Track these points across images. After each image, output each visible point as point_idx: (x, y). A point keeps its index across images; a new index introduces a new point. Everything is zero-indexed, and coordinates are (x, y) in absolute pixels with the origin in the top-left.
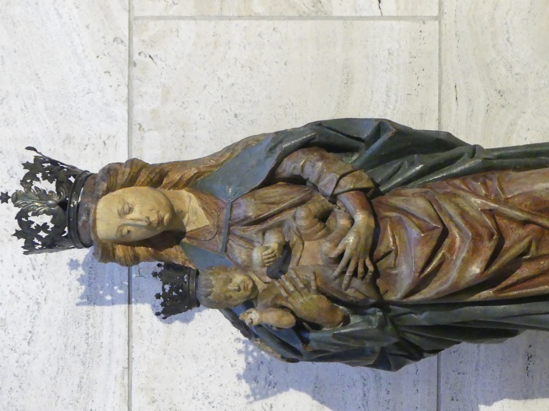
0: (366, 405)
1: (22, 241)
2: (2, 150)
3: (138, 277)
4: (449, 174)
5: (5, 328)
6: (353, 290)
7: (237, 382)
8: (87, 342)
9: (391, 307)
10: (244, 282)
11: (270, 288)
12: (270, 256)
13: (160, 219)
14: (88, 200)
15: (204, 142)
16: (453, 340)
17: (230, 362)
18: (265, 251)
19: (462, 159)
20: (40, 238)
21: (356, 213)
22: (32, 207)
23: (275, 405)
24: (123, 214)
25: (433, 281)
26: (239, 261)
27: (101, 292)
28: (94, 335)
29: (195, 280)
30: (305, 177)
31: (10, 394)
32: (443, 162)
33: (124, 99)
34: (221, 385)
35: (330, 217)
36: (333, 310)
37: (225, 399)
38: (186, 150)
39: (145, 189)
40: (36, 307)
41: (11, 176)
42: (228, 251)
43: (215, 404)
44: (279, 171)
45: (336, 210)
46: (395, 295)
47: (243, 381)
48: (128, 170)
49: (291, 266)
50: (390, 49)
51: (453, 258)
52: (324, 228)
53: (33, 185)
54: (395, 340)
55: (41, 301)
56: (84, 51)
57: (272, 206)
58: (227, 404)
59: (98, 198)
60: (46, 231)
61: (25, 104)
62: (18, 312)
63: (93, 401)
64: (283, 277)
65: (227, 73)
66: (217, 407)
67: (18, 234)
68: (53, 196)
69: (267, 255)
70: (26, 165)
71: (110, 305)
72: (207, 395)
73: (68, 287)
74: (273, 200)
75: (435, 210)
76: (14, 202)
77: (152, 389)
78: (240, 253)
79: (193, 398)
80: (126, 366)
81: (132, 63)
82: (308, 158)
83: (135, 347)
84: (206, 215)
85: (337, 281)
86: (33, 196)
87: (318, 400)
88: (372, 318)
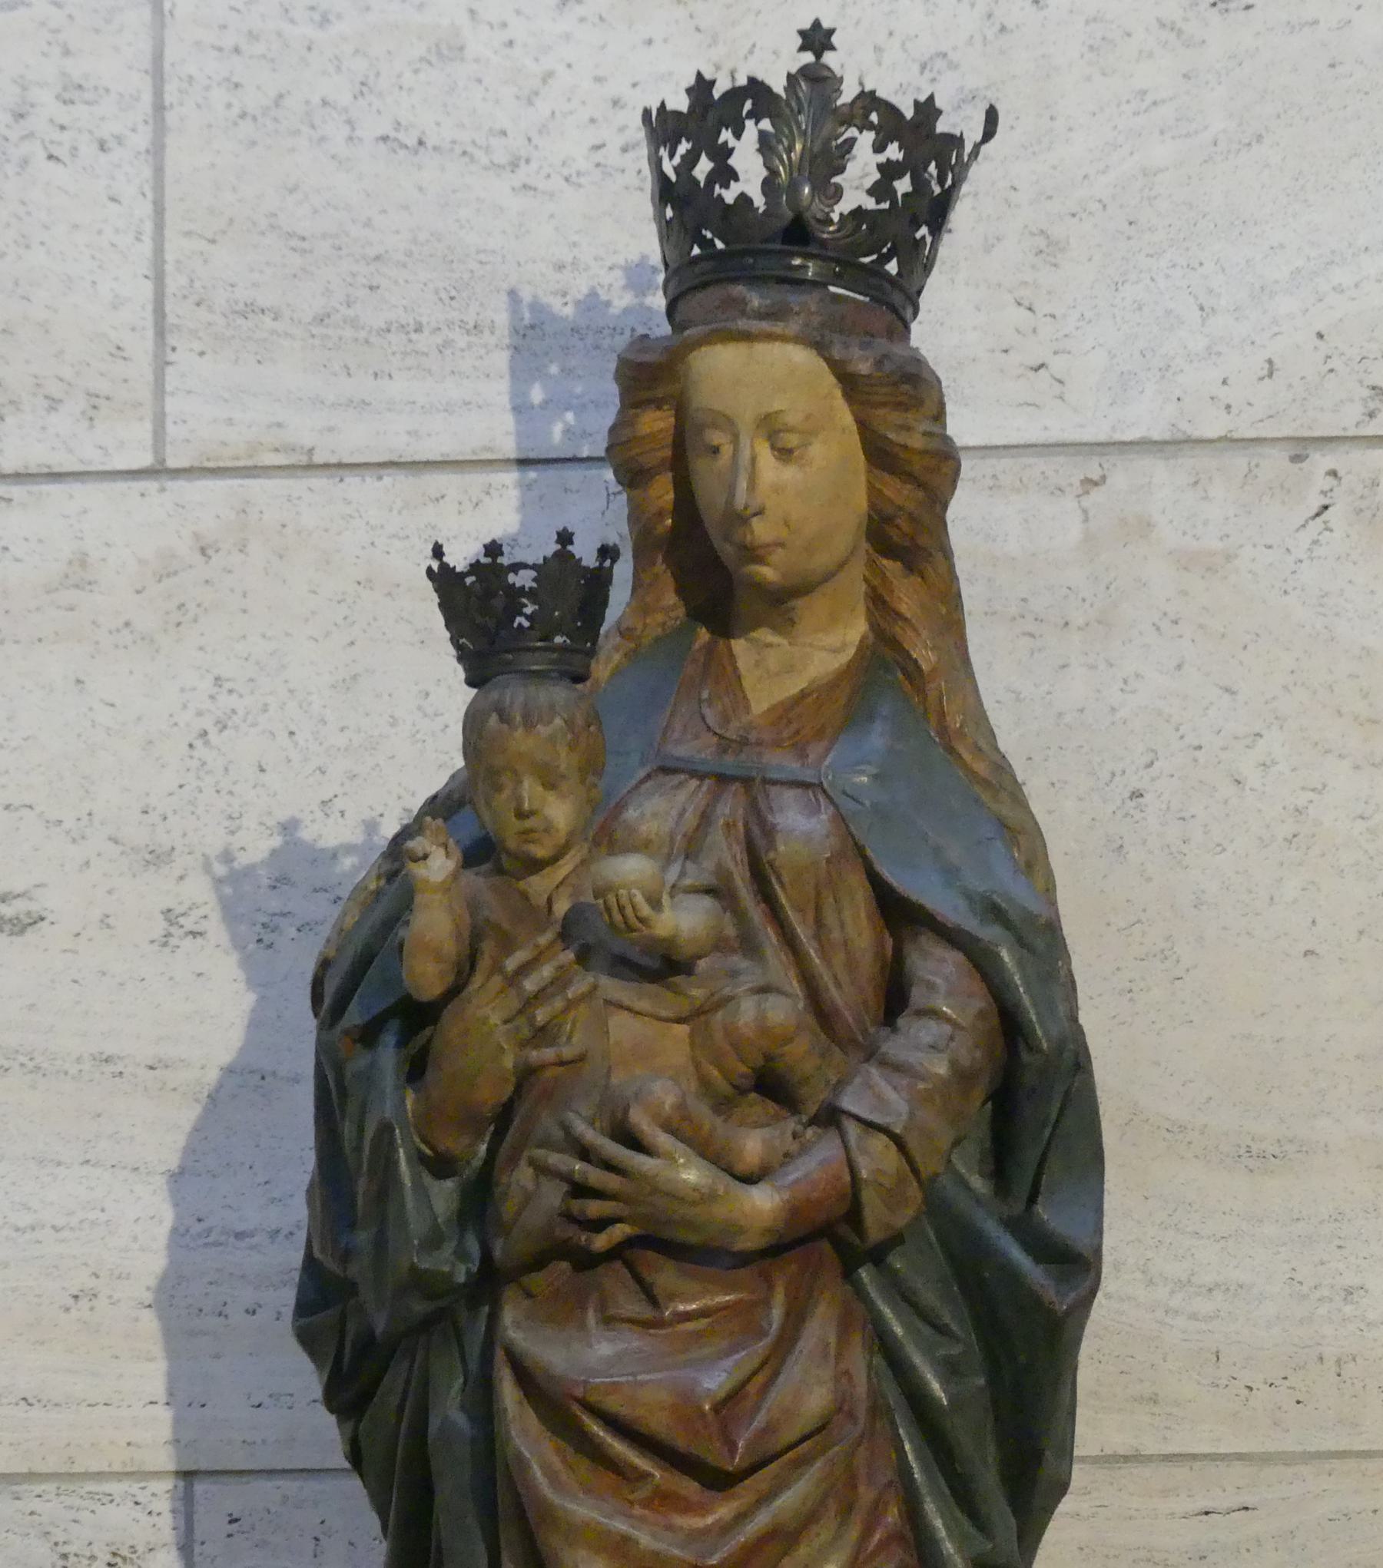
0: (207, 1241)
1: (680, 103)
2: (1012, 31)
3: (607, 488)
4: (917, 1488)
5: (434, 59)
6: (530, 1186)
7: (271, 822)
8: (393, 329)
9: (486, 1309)
10: (547, 830)
11: (536, 915)
12: (629, 911)
13: (761, 552)
14: (812, 313)
15: (1049, 693)
16: (392, 1514)
17: (336, 796)
18: (643, 894)
19: (973, 1531)
20: (691, 160)
21: (778, 1189)
22: (786, 131)
23: (203, 947)
24: (771, 427)
25: (563, 1444)
26: (631, 814)
27: (554, 369)
28: (417, 352)
29: (554, 671)
30: (901, 1022)
31: (219, 84)
32: (959, 1470)
33: (1184, 426)
34: (262, 770)
35: (772, 1107)
36: (470, 1122)
37: (217, 783)
38: (1024, 634)
39: (860, 501)
40: (502, 158)
41: (926, 64)
42: (661, 778)
43: (201, 751)
44: (923, 939)
45: (791, 1124)
46: (517, 1325)
47: (277, 841)
48: (916, 442)
49: (605, 981)
50: (1366, 1292)
51: (637, 1507)
52: (735, 1087)
53: (861, 132)
54: (380, 1325)
55: (523, 174)
56: (1339, 289)
57: (811, 916)
58: (201, 791)
59: (820, 347)
60: (711, 179)
61: (1163, 101)
62: (484, 99)
63: (202, 354)
64: (569, 956)
65: (1274, 763)
66: (191, 757)
67: (701, 87)
68: (823, 198)
69: (631, 900)
70: (927, 110)
71: (511, 399)
72: (230, 724)
73: (570, 259)
74: (830, 918)
75: (791, 1447)
76: (804, 71)
77: (245, 546)
78: (655, 815)
79: (217, 679)
80: (319, 458)
81: (1301, 447)
82: (962, 1028)
83: (378, 484)
84: (782, 703)
85: (558, 1134)
86: (825, 132)
87: (220, 1086)
88: (448, 1249)
